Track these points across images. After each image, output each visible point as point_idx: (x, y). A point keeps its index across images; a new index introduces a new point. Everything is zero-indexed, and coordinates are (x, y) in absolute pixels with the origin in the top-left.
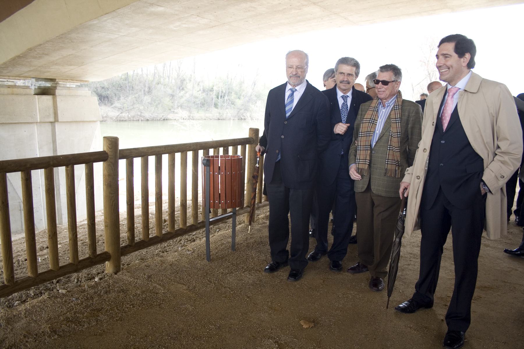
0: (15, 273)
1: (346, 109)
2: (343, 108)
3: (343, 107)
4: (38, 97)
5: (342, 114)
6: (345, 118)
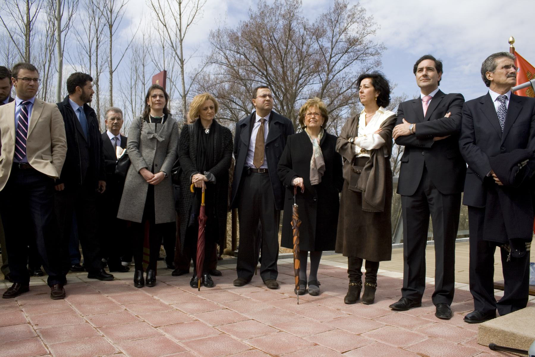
0: (144, 121)
1: (505, 110)
2: (500, 111)
3: (500, 109)
4: (132, 284)
5: (500, 117)
6: (503, 121)
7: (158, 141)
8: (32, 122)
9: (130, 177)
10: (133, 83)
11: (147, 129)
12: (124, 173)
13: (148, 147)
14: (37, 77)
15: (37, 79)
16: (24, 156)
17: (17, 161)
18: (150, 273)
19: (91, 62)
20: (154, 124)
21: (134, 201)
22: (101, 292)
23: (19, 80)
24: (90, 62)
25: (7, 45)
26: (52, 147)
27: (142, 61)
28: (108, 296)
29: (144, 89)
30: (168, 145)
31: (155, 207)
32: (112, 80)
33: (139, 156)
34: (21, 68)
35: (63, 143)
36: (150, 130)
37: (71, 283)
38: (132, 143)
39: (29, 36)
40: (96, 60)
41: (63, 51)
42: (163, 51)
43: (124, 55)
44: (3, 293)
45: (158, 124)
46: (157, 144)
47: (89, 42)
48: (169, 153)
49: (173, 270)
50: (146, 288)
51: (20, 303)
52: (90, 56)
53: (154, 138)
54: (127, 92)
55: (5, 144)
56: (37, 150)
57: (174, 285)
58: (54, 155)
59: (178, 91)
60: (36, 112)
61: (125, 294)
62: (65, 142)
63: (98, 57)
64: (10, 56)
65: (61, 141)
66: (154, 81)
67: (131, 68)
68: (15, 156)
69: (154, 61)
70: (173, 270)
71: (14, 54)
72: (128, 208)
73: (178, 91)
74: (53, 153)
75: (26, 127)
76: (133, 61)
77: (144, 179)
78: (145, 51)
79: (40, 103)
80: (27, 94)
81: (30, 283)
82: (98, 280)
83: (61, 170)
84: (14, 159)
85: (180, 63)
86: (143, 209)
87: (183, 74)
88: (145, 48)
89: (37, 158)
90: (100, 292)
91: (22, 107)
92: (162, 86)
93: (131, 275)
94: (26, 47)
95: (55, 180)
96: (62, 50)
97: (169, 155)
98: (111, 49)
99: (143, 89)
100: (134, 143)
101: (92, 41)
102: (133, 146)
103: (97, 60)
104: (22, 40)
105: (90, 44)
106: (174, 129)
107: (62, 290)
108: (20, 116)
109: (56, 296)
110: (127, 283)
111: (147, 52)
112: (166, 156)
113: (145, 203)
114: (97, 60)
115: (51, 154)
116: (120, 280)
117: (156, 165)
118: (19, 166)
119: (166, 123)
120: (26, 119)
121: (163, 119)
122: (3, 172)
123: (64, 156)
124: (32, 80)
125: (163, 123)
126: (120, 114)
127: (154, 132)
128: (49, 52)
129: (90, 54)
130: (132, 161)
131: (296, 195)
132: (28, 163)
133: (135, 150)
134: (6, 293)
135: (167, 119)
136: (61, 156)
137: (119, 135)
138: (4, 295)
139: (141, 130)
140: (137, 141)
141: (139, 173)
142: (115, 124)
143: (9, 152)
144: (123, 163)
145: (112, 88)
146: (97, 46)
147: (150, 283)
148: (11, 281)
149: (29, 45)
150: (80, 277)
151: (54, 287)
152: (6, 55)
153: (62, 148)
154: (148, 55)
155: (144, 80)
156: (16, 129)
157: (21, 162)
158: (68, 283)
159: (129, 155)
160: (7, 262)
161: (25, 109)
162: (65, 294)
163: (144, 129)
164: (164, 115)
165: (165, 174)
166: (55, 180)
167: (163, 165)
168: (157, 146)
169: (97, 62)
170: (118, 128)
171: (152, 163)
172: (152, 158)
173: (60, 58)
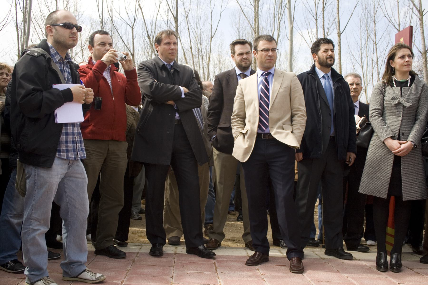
7: (404, 106)
8: (273, 93)
9: (373, 148)
10: (363, 43)
11: (391, 94)
12: (366, 144)
13: (392, 113)
14: (275, 47)
15: (275, 49)
16: (267, 127)
17: (260, 132)
18: (394, 256)
19: (318, 25)
20: (399, 88)
21: (378, 175)
22: (340, 271)
23: (259, 52)
24: (317, 26)
25: (238, 19)
26: (292, 116)
27: (373, 18)
28: (348, 277)
29: (376, 49)
30: (417, 111)
31: (402, 182)
32: (340, 42)
33: (383, 124)
34: (260, 40)
35: (303, 112)
36: (395, 96)
37: (308, 258)
38: (374, 111)
39: (258, 7)
40: (322, 22)
41: (294, 18)
42: (397, 3)
43: (352, 14)
44: (246, 260)
45: (403, 88)
46: (403, 110)
47: (315, 4)
48: (417, 120)
49: (421, 256)
50: (391, 273)
51: (261, 272)
52: (316, 20)
53: (399, 104)
54: (357, 54)
55: (250, 116)
56: (279, 120)
57: (423, 274)
58: (294, 125)
59: (417, 48)
60: (276, 83)
61: (268, 265)
62: (305, 111)
63: (325, 19)
64: (240, 29)
65: (300, 111)
66: (397, 39)
67: (360, 27)
68: (259, 127)
69: (387, 16)
70: (421, 256)
71: (244, 27)
72: (372, 182)
73: (417, 48)
74: (293, 123)
75: (268, 97)
76: (362, 19)
77: (389, 150)
78: (376, 7)
79: (280, 73)
80: (266, 65)
81: (270, 253)
82: (336, 258)
83: (301, 139)
84: (258, 130)
85: (418, 15)
86: (389, 183)
87: (423, 27)
88: (375, 3)
89: (278, 128)
90: (339, 271)
91: (263, 78)
92: (408, 46)
93: (372, 255)
94: (256, 18)
95: (295, 150)
96: (292, 17)
97: (418, 122)
98: (338, 9)
99: (375, 48)
100: (377, 110)
101: (318, 3)
102: (375, 114)
103: (324, 23)
104: (251, 12)
105: (316, 7)
106: (423, 92)
107: (300, 264)
108: (261, 87)
109: (295, 269)
110: (367, 265)
111: (379, 6)
112: (414, 124)
113: (390, 176)
114: (324, 23)
115: (291, 124)
116: (359, 260)
117: (403, 134)
118: (262, 136)
119: (413, 86)
120: (268, 90)
121: (409, 82)
122: (248, 143)
123: (304, 125)
124: (270, 51)
125: (410, 86)
126: (359, 79)
127: (399, 97)
128: (278, 20)
129: (317, 17)
130: (375, 130)
131: (82, 134)
132: (270, 134)
133: (378, 118)
134: (248, 260)
135: (415, 81)
136: (301, 125)
137: (358, 102)
138: (247, 262)
139: (384, 96)
140: (380, 108)
141: (384, 143)
142: (354, 89)
143: (254, 123)
144: (365, 133)
145: (340, 51)
146: (324, 7)
147: (395, 268)
148: (251, 249)
149: (258, 16)
150: (316, 253)
151: (293, 260)
152: (237, 29)
153: (302, 117)
154: (379, 10)
155: (376, 39)
156: (259, 100)
157: (264, 132)
158: (305, 257)
159: (372, 124)
160: (249, 230)
161: (266, 80)
162: (303, 268)
163: (387, 94)
164: (410, 77)
165: (414, 144)
166: (295, 150)
167: (411, 134)
168: (403, 113)
169: (324, 25)
170: (357, 94)
171: (398, 131)
172: (398, 127)
173: (291, 25)
